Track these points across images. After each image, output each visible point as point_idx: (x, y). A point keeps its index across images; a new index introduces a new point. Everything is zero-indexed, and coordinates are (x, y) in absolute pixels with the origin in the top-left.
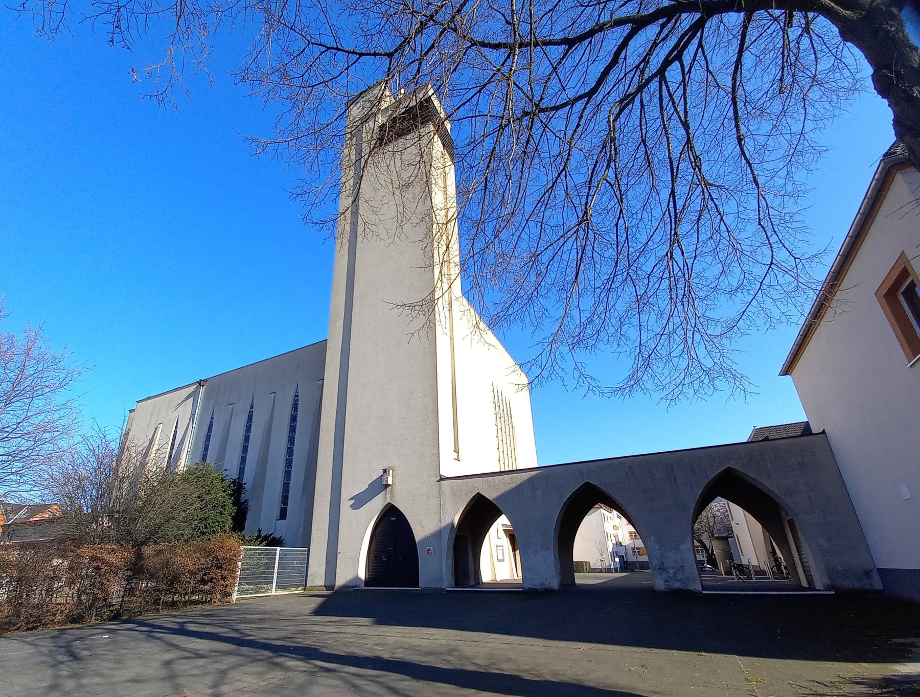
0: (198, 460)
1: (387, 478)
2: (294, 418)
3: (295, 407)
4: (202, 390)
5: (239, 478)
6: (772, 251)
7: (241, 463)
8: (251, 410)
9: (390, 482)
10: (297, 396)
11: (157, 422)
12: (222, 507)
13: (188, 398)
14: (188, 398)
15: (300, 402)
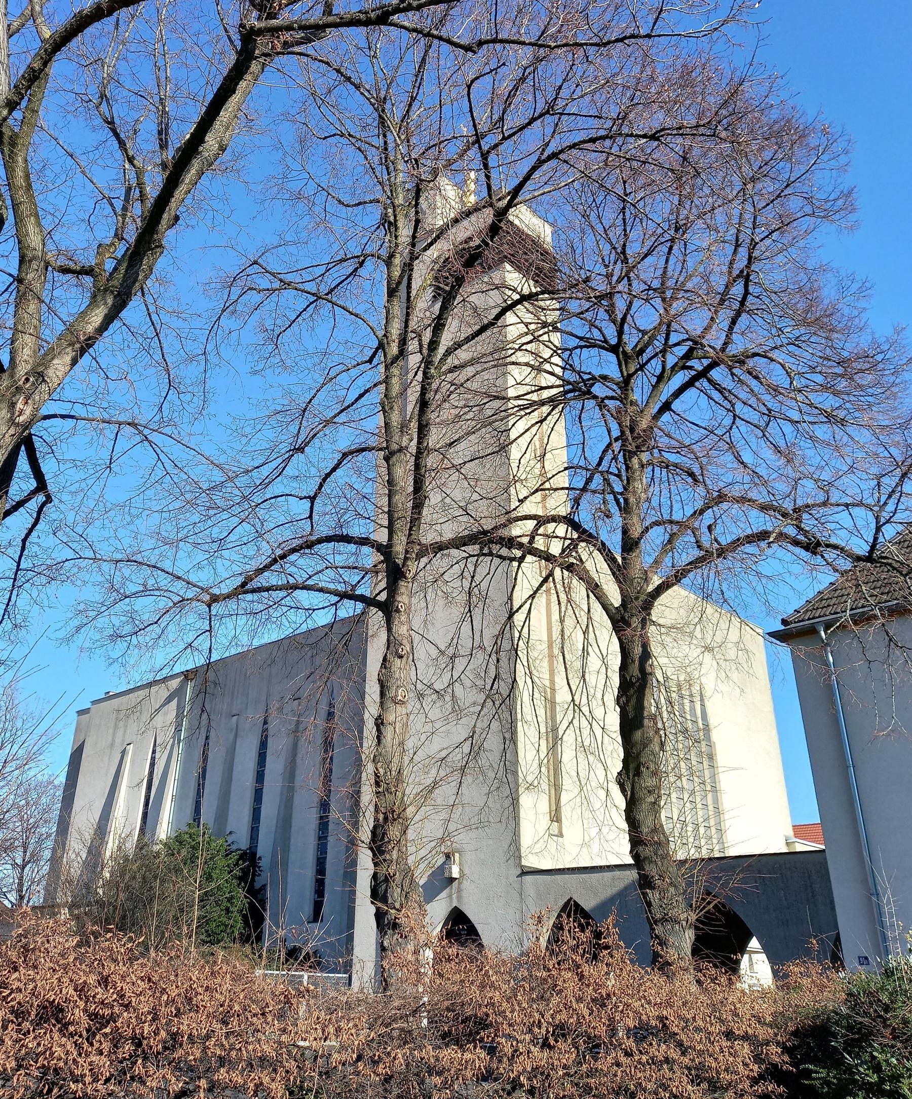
0: (188, 817)
1: (451, 868)
4: (190, 686)
5: (250, 848)
6: (750, 406)
7: (253, 820)
9: (455, 873)
11: (123, 740)
12: (228, 901)
13: (169, 700)
14: (169, 700)
15: (327, 882)
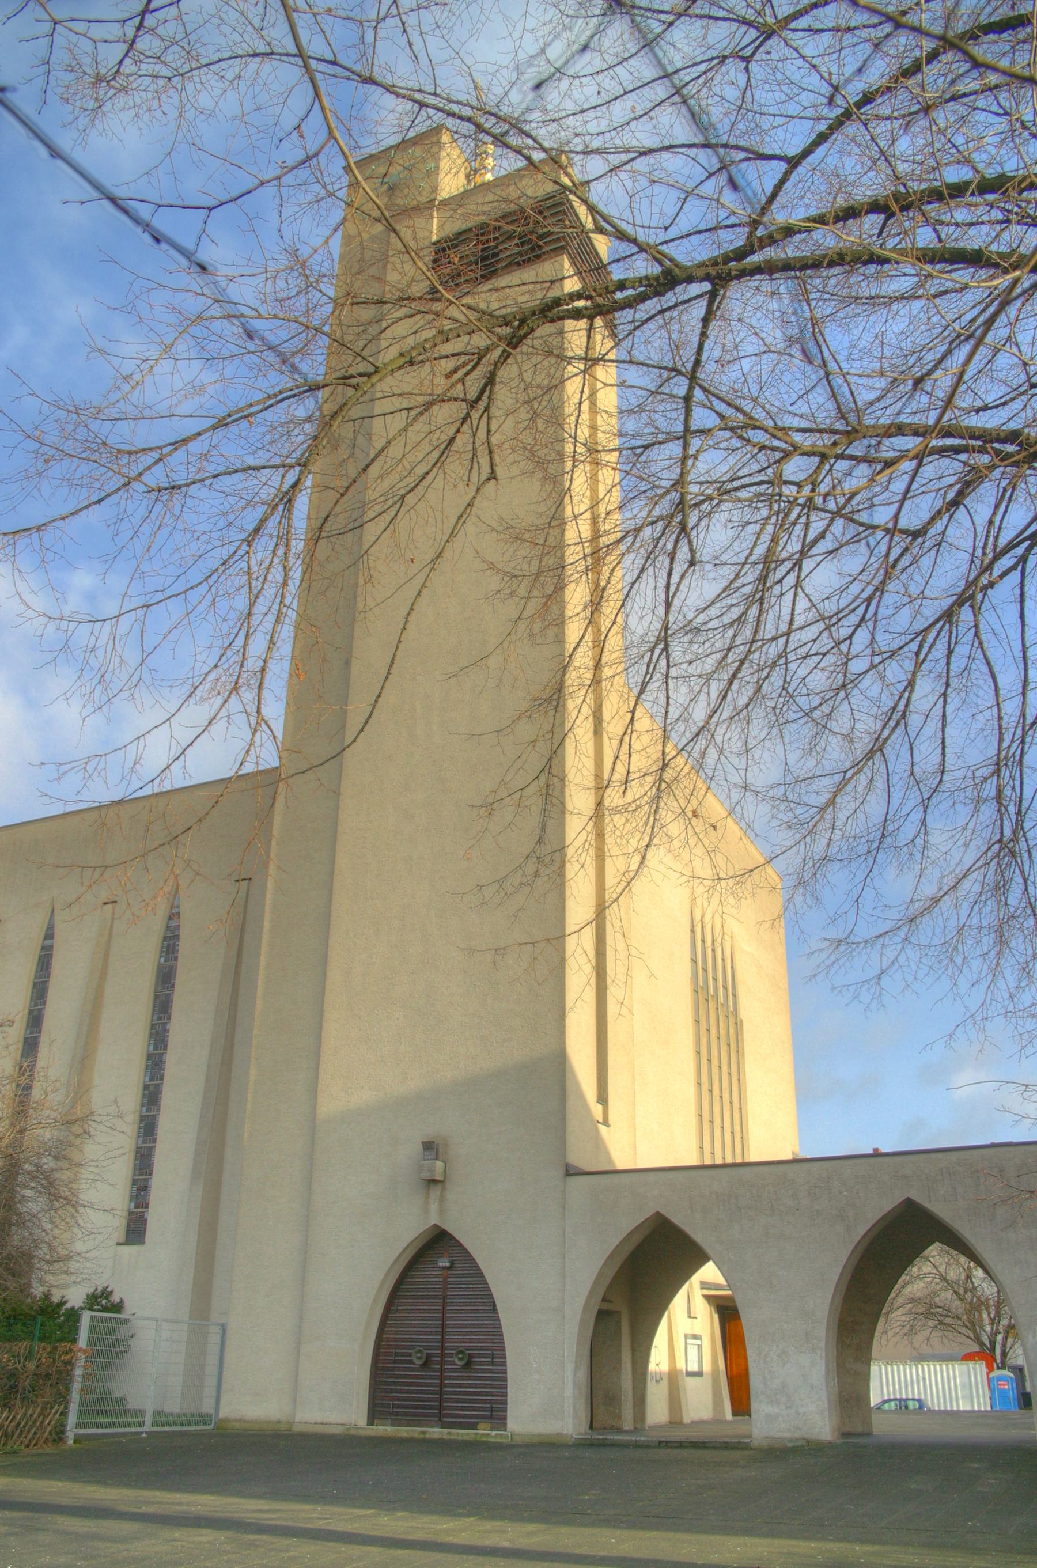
2: (166, 978)
8: (48, 942)
15: (184, 933)
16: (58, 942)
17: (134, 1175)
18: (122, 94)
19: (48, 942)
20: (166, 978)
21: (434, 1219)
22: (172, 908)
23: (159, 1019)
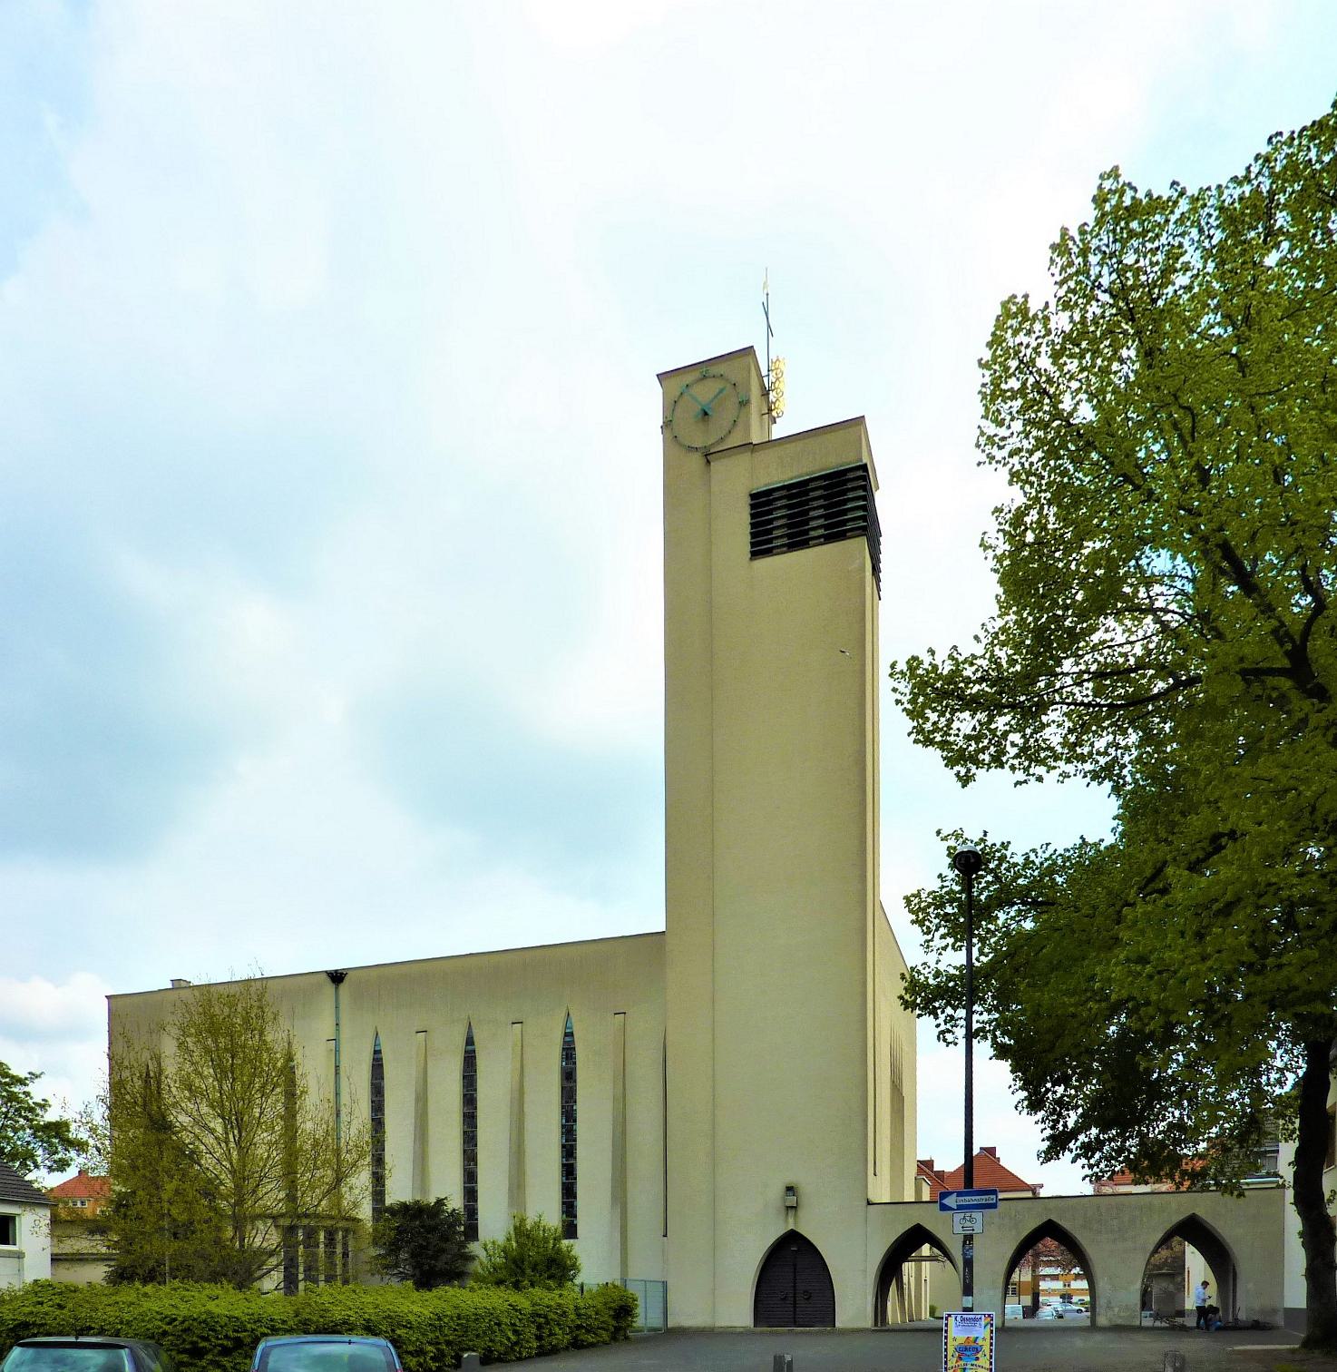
2: (569, 1076)
3: (569, 1053)
8: (470, 1048)
10: (572, 1034)
16: (478, 1047)
17: (563, 1198)
18: (1058, 240)
19: (470, 1048)
20: (569, 1076)
21: (791, 1226)
22: (566, 1028)
23: (567, 1102)
